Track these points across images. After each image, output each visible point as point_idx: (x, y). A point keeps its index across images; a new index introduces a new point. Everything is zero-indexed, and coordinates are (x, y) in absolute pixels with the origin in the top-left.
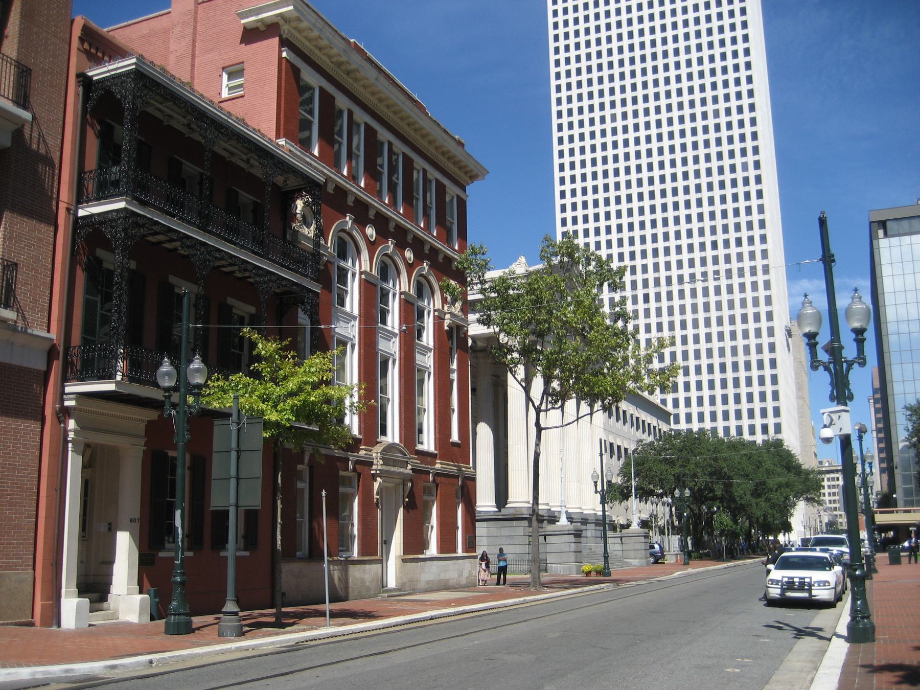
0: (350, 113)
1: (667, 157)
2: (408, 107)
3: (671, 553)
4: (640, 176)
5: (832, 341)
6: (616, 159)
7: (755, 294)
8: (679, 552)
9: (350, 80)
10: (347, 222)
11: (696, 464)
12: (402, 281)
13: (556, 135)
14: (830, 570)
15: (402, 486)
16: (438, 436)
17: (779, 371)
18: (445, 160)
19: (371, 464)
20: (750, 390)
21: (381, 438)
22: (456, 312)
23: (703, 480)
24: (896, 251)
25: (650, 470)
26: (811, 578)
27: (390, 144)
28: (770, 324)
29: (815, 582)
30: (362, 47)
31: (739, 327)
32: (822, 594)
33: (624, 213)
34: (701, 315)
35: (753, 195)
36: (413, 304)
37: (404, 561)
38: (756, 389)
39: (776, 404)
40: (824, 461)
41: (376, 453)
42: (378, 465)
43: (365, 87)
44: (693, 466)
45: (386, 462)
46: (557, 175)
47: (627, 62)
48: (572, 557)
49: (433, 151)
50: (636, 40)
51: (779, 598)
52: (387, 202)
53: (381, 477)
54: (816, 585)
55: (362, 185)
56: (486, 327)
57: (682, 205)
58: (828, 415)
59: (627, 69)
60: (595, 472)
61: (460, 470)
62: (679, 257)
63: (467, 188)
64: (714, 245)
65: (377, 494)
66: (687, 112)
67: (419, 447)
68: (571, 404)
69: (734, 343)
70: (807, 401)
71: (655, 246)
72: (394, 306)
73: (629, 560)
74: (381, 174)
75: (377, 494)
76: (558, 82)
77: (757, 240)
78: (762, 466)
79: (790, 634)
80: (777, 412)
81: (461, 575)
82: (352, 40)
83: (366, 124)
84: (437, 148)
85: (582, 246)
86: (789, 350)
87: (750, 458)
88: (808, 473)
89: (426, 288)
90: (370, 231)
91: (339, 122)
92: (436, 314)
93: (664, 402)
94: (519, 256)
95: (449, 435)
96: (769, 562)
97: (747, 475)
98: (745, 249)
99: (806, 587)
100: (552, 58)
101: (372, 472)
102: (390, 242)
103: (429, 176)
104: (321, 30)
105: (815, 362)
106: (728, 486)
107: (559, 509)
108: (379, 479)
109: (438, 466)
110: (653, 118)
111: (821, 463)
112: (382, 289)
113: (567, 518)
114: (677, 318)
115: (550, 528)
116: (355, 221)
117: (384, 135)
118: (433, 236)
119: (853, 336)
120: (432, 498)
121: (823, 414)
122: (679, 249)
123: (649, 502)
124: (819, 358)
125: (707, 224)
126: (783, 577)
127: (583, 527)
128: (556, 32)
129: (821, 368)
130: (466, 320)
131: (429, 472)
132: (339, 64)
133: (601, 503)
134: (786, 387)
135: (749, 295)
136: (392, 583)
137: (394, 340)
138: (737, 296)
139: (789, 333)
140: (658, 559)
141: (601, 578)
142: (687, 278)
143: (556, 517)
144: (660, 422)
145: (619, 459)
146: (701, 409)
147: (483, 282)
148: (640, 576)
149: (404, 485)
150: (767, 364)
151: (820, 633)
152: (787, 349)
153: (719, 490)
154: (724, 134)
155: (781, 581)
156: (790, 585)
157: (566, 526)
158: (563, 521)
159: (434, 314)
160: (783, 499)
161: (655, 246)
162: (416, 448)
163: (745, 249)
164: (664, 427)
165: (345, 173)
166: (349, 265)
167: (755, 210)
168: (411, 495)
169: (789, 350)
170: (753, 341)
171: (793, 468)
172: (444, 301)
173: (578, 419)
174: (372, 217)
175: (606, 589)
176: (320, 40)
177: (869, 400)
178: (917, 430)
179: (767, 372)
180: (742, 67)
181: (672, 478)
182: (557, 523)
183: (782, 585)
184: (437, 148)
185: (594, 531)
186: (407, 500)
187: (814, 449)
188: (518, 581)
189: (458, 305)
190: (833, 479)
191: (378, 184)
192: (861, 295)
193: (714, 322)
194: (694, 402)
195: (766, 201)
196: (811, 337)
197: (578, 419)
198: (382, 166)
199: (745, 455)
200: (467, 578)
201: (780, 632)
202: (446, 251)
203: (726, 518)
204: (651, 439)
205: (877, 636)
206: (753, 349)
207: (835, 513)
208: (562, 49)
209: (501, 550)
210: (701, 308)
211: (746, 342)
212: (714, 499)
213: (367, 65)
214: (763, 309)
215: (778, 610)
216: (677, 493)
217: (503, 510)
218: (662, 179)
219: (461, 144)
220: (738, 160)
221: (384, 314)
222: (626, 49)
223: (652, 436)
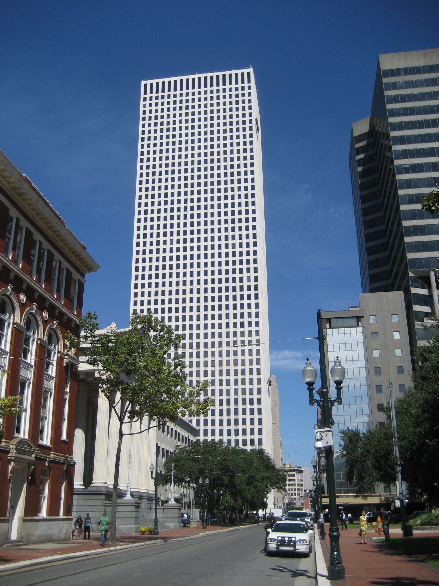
0: (18, 220)
1: (202, 269)
2: (54, 221)
3: (194, 520)
4: (185, 279)
5: (322, 388)
6: (157, 268)
7: (251, 357)
8: (199, 520)
9: (20, 199)
10: (8, 290)
11: (212, 462)
12: (39, 331)
13: (135, 248)
14: (306, 533)
15: (27, 469)
16: (53, 435)
17: (262, 406)
18: (74, 257)
19: (8, 452)
20: (244, 417)
21: (17, 435)
22: (72, 355)
23: (216, 473)
24: (336, 336)
25: (183, 465)
26: (295, 538)
27: (41, 243)
28: (259, 376)
29: (297, 540)
30: (30, 180)
31: (240, 377)
32: (302, 548)
33: (174, 301)
34: (217, 368)
35: (253, 297)
36: (45, 347)
37: (24, 521)
38: (248, 417)
39: (260, 427)
40: (287, 464)
41: (12, 445)
42: (13, 453)
43: (29, 205)
44: (210, 464)
45: (19, 451)
46: (134, 273)
47: (182, 209)
48: (133, 521)
49: (67, 250)
50: (189, 197)
51: (275, 551)
52: (35, 279)
53: (14, 461)
54: (298, 542)
55: (20, 267)
56: (92, 366)
57: (209, 299)
58: (320, 433)
59: (182, 213)
60: (152, 465)
61: (66, 459)
62: (206, 331)
63: (86, 275)
64: (228, 325)
65: (10, 473)
66: (216, 243)
67: (41, 442)
68: (146, 419)
69: (236, 387)
70: (278, 426)
71: (191, 323)
72: (33, 348)
73: (168, 525)
74: (33, 261)
75: (10, 473)
76: (139, 217)
77: (253, 324)
78: (253, 466)
79: (289, 574)
80: (260, 432)
81: (61, 532)
82: (24, 175)
83: (27, 229)
84: (69, 249)
85: (159, 319)
86: (269, 393)
87: (246, 460)
88: (279, 471)
89: (54, 338)
90: (22, 297)
91: (10, 225)
92: (59, 355)
93: (191, 421)
94: (112, 322)
95: (60, 435)
96: (268, 527)
97: (244, 471)
98: (246, 329)
99: (292, 544)
100: (137, 201)
101: (9, 458)
102: (34, 306)
103: (63, 266)
104: (6, 165)
105: (312, 400)
106: (232, 477)
107: (126, 489)
108: (13, 463)
109: (52, 456)
110: (195, 244)
111: (284, 465)
112: (26, 335)
113: (131, 495)
114: (202, 369)
115: (119, 501)
116: (13, 290)
117: (37, 237)
118: (61, 304)
119: (307, 386)
120: (45, 478)
121: (317, 432)
122: (206, 326)
123: (180, 486)
124: (315, 398)
125: (195, 313)
126: (278, 537)
127: (140, 501)
128: (141, 186)
129: (316, 404)
130: (77, 361)
131: (45, 460)
132: (14, 189)
133: (154, 486)
134: (267, 416)
135: (247, 357)
136: (14, 536)
137: (30, 370)
138: (239, 358)
139: (270, 383)
140: (186, 524)
141: (153, 536)
142: (246, 343)
143: (123, 494)
144: (190, 435)
145: (163, 457)
146: (213, 428)
147: (94, 336)
148: (177, 535)
149: (29, 467)
150: (255, 401)
151: (307, 574)
152: (268, 392)
153: (226, 480)
154: (237, 258)
155: (277, 540)
156: (282, 542)
157: (130, 500)
158: (128, 497)
159: (58, 354)
160: (264, 487)
161: (191, 323)
162: (39, 443)
163: (246, 329)
164: (193, 439)
165: (10, 258)
166: (7, 317)
167: (253, 306)
168: (33, 475)
169: (269, 393)
170: (248, 387)
171: (271, 467)
172: (65, 346)
173: (148, 429)
174: (24, 288)
175: (159, 544)
176: (4, 172)
177: (315, 426)
178: (347, 446)
179: (256, 406)
180: (250, 220)
181: (197, 471)
182: (124, 498)
183: (277, 542)
184: (69, 249)
185: (146, 504)
186: (30, 478)
187: (281, 456)
188: (97, 537)
189: (73, 350)
190: (291, 476)
191: (31, 266)
192: (311, 362)
193: (224, 373)
194: (225, 422)
195: (260, 301)
196: (310, 384)
197: (148, 429)
198: (34, 256)
199: (243, 458)
200: (65, 534)
201: (282, 573)
202: (69, 314)
203: (229, 497)
204: (183, 445)
205: (346, 576)
206: (248, 392)
207: (292, 497)
208: (143, 197)
209: (88, 515)
210: (217, 363)
211: (243, 387)
212: (221, 486)
213: (32, 191)
214: (255, 367)
215: (274, 558)
216: (201, 481)
217: (89, 488)
218: (199, 282)
219: (84, 248)
220: (245, 275)
221: (26, 352)
222: (182, 201)
223: (184, 443)
